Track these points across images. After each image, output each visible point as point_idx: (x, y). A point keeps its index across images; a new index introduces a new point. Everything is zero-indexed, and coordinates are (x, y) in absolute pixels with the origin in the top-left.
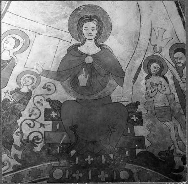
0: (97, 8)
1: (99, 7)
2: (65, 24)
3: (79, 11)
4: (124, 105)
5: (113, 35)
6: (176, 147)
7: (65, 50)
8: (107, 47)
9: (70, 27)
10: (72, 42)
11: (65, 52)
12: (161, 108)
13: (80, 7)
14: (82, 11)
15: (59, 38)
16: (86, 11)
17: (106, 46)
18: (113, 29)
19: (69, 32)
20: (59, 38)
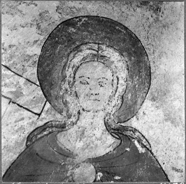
0: (117, 28)
1: (121, 24)
2: (30, 57)
3: (72, 30)
4: (42, 89)
5: (153, 99)
6: (145, 144)
7: (22, 138)
8: (137, 134)
9: (44, 70)
10: (43, 115)
11: (21, 144)
12: (113, 21)
13: (76, 18)
14: (79, 29)
15: (8, 98)
16: (88, 31)
17: (135, 130)
18: (153, 82)
19: (38, 83)
20: (8, 98)
